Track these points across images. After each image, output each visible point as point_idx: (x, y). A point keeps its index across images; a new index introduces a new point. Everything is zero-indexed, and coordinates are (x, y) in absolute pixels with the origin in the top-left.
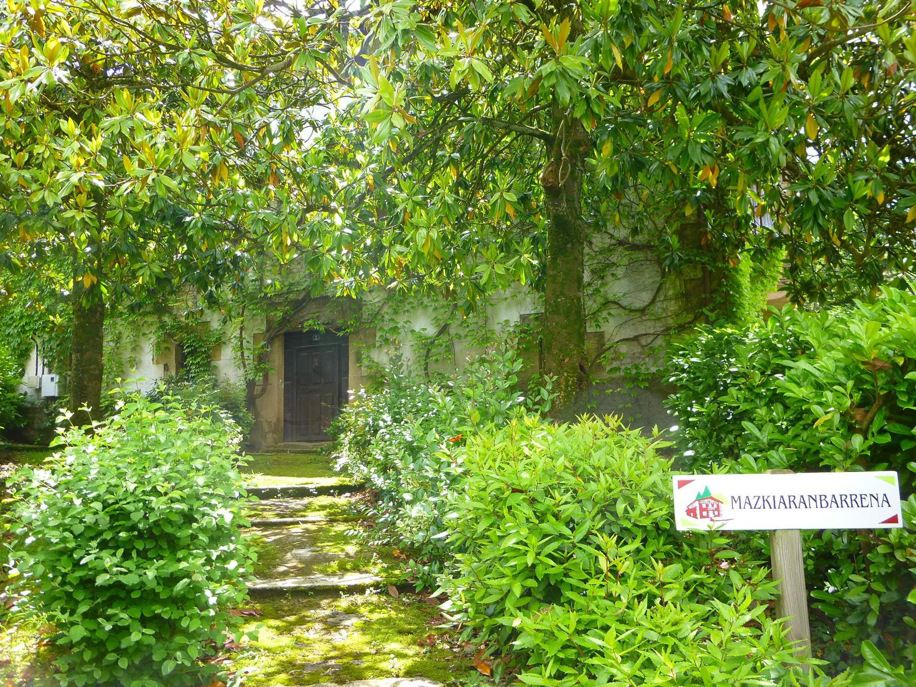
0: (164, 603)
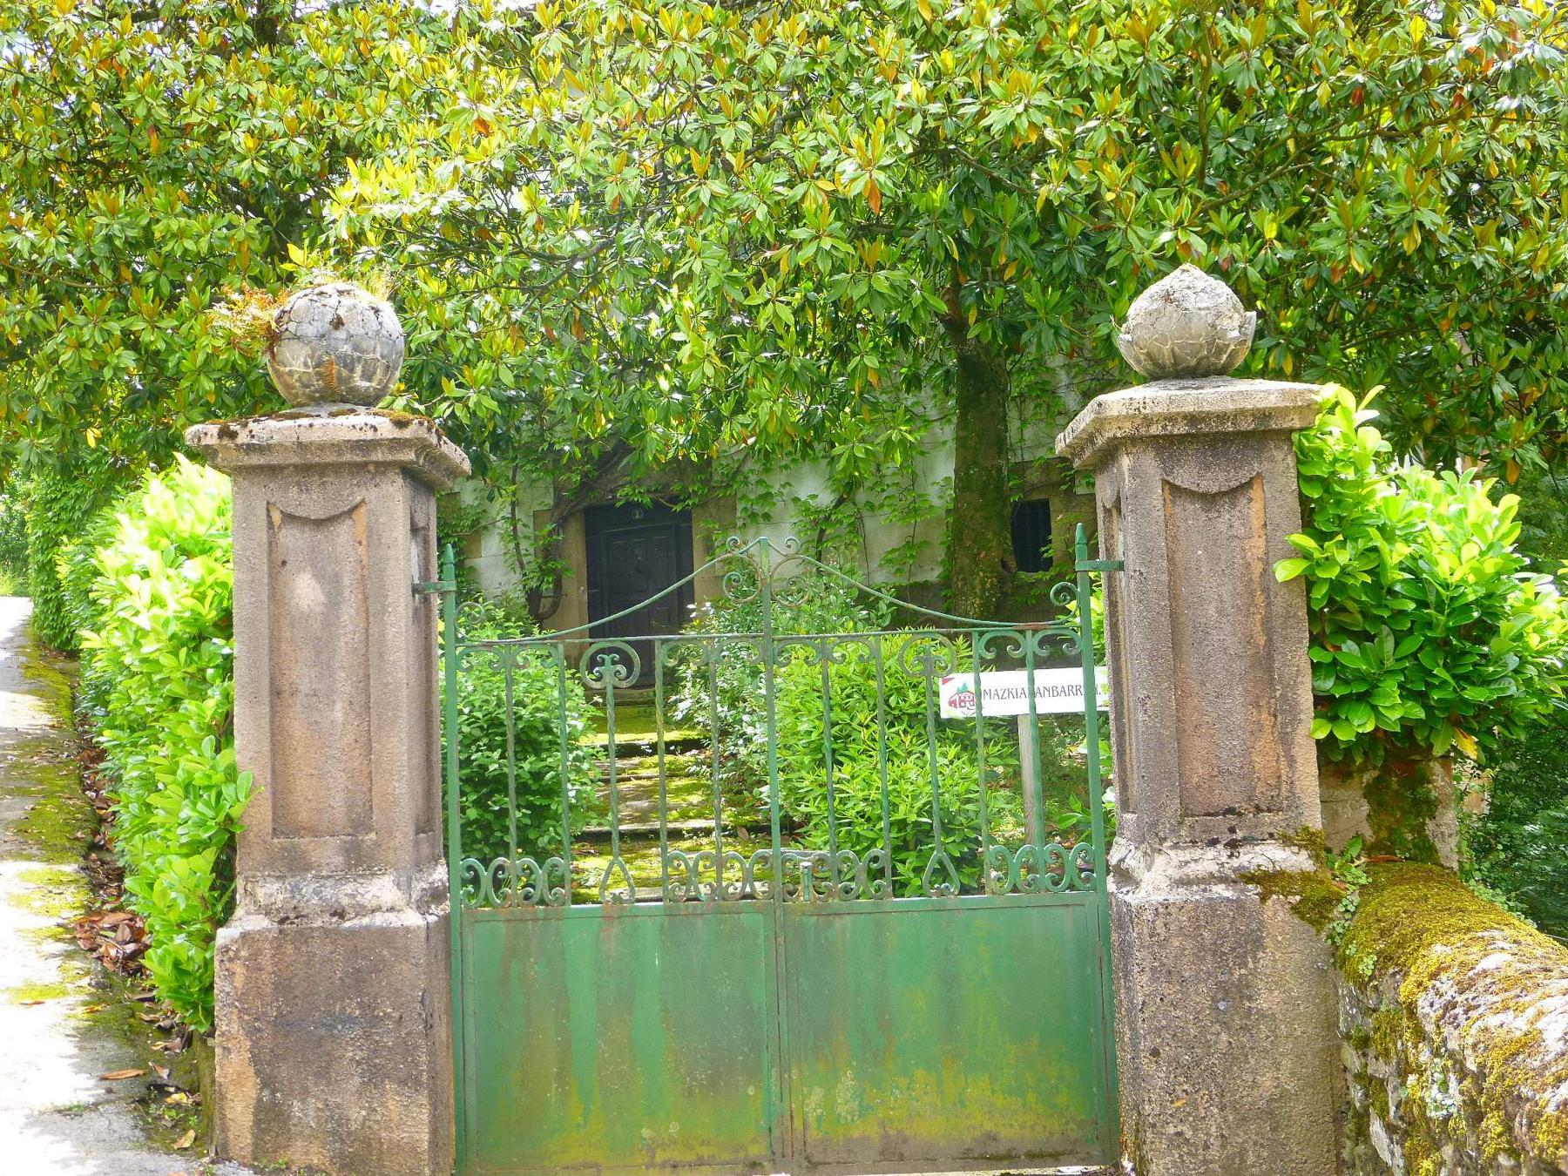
0: (534, 793)
